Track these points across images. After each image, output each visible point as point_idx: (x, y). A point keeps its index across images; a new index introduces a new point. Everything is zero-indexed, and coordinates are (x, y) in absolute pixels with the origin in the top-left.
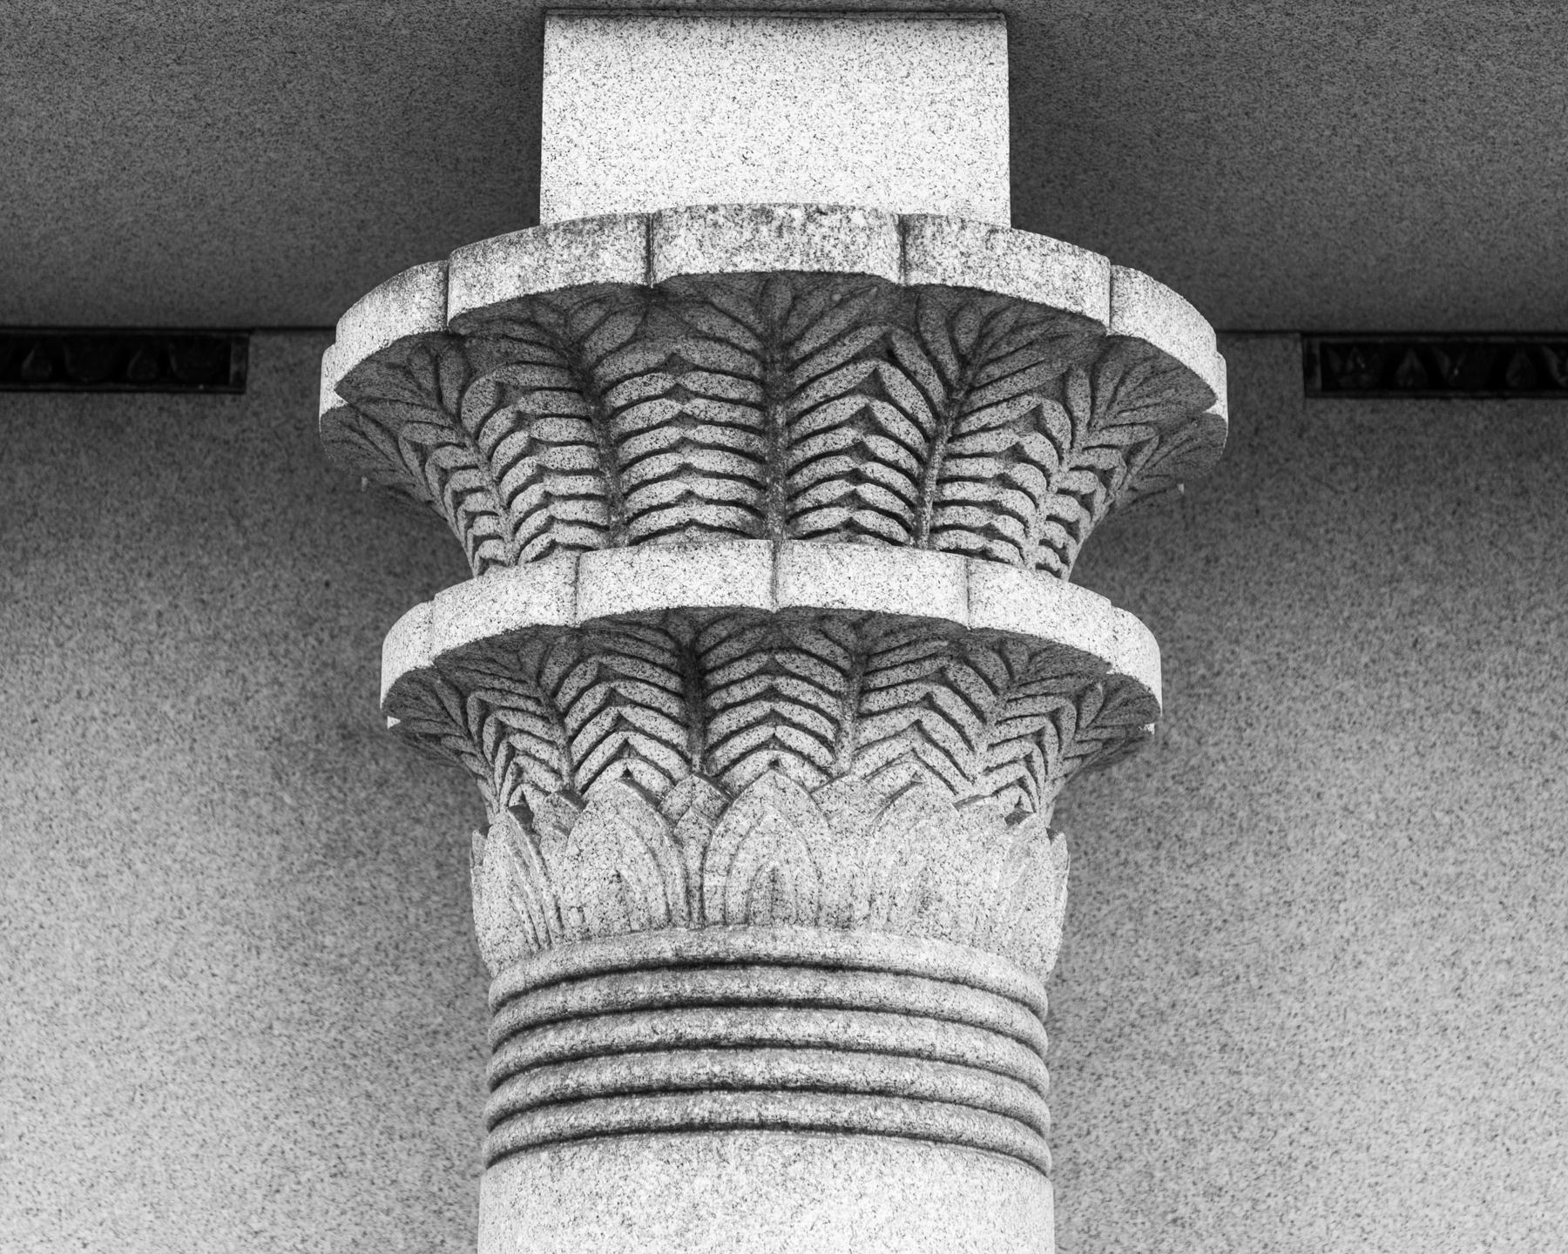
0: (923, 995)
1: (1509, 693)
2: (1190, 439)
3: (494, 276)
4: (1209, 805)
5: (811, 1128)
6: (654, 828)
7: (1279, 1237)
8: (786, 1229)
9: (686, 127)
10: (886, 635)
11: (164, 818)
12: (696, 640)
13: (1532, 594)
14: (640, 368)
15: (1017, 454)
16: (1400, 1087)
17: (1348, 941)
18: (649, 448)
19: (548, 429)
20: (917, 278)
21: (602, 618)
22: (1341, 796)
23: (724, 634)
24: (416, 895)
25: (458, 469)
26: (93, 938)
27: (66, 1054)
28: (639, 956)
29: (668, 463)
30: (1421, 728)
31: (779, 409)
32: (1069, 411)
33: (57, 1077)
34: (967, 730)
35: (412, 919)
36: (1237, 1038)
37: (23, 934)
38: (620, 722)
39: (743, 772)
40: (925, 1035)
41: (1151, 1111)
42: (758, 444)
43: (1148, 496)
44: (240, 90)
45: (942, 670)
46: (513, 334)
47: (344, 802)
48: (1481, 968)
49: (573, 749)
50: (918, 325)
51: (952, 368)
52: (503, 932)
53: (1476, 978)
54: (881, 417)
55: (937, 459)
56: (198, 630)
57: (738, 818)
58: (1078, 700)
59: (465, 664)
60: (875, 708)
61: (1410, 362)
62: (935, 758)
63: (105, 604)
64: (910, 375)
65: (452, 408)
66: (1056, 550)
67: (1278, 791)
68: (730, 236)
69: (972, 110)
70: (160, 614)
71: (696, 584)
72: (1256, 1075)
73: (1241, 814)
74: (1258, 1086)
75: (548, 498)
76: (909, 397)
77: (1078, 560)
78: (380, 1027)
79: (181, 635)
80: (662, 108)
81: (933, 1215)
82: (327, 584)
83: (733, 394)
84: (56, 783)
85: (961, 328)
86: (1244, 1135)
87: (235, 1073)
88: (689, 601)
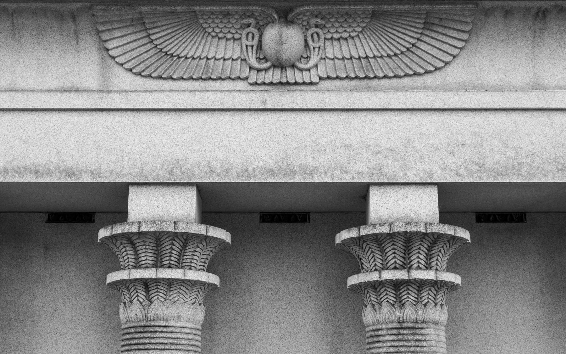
0: (178, 330)
3: (119, 229)
4: (241, 288)
5: (161, 349)
6: (141, 307)
15: (195, 251)
19: (128, 249)
20: (176, 231)
29: (144, 254)
38: (137, 292)
39: (154, 299)
40: (179, 335)
42: (156, 252)
51: (184, 241)
56: (87, 262)
57: (152, 306)
61: (276, 217)
62: (181, 296)
68: (150, 226)
74: (247, 332)
76: (178, 245)
84: (65, 286)
87: (93, 331)
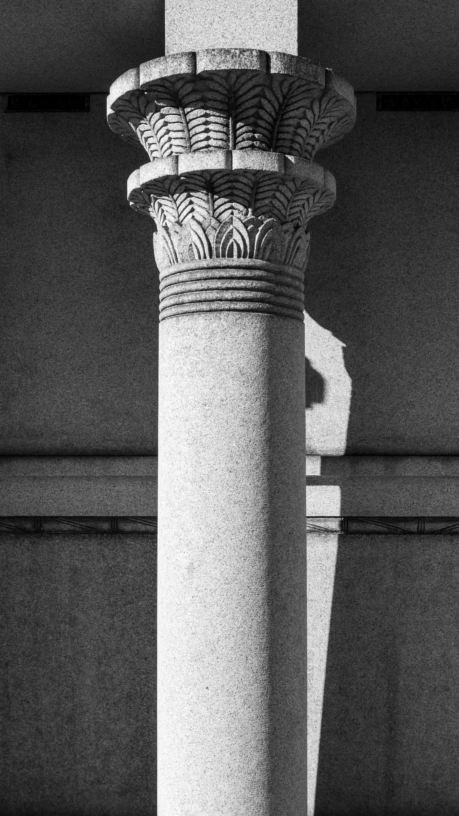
1: (426, 193)
2: (346, 121)
3: (152, 72)
7: (361, 334)
8: (237, 336)
9: (207, 26)
10: (263, 177)
11: (75, 231)
12: (211, 179)
13: (433, 166)
14: (194, 100)
16: (392, 297)
17: (381, 260)
18: (197, 124)
21: (185, 173)
22: (381, 221)
23: (219, 177)
24: (142, 251)
25: (145, 131)
26: (59, 263)
27: (54, 293)
28: (198, 266)
30: (403, 203)
31: (233, 111)
32: (313, 112)
33: (53, 299)
34: (284, 203)
35: (141, 257)
36: (352, 285)
37: (41, 262)
41: (330, 304)
43: (334, 138)
44: (79, 17)
45: (278, 187)
46: (158, 90)
47: (122, 226)
48: (414, 266)
49: (179, 210)
50: (271, 86)
52: (162, 260)
53: (413, 269)
54: (261, 114)
55: (277, 126)
58: (314, 195)
59: (149, 186)
60: (260, 198)
63: (56, 172)
64: (269, 101)
65: (143, 113)
66: (309, 153)
67: (365, 220)
68: (218, 59)
69: (287, 21)
70: (71, 175)
71: (210, 163)
72: (357, 294)
73: (356, 226)
75: (170, 139)
76: (269, 108)
77: (315, 156)
78: (134, 285)
79: (77, 181)
80: (199, 20)
81: (274, 332)
82: (115, 166)
83: (220, 107)
85: (283, 86)
86: (353, 309)
88: (209, 167)
